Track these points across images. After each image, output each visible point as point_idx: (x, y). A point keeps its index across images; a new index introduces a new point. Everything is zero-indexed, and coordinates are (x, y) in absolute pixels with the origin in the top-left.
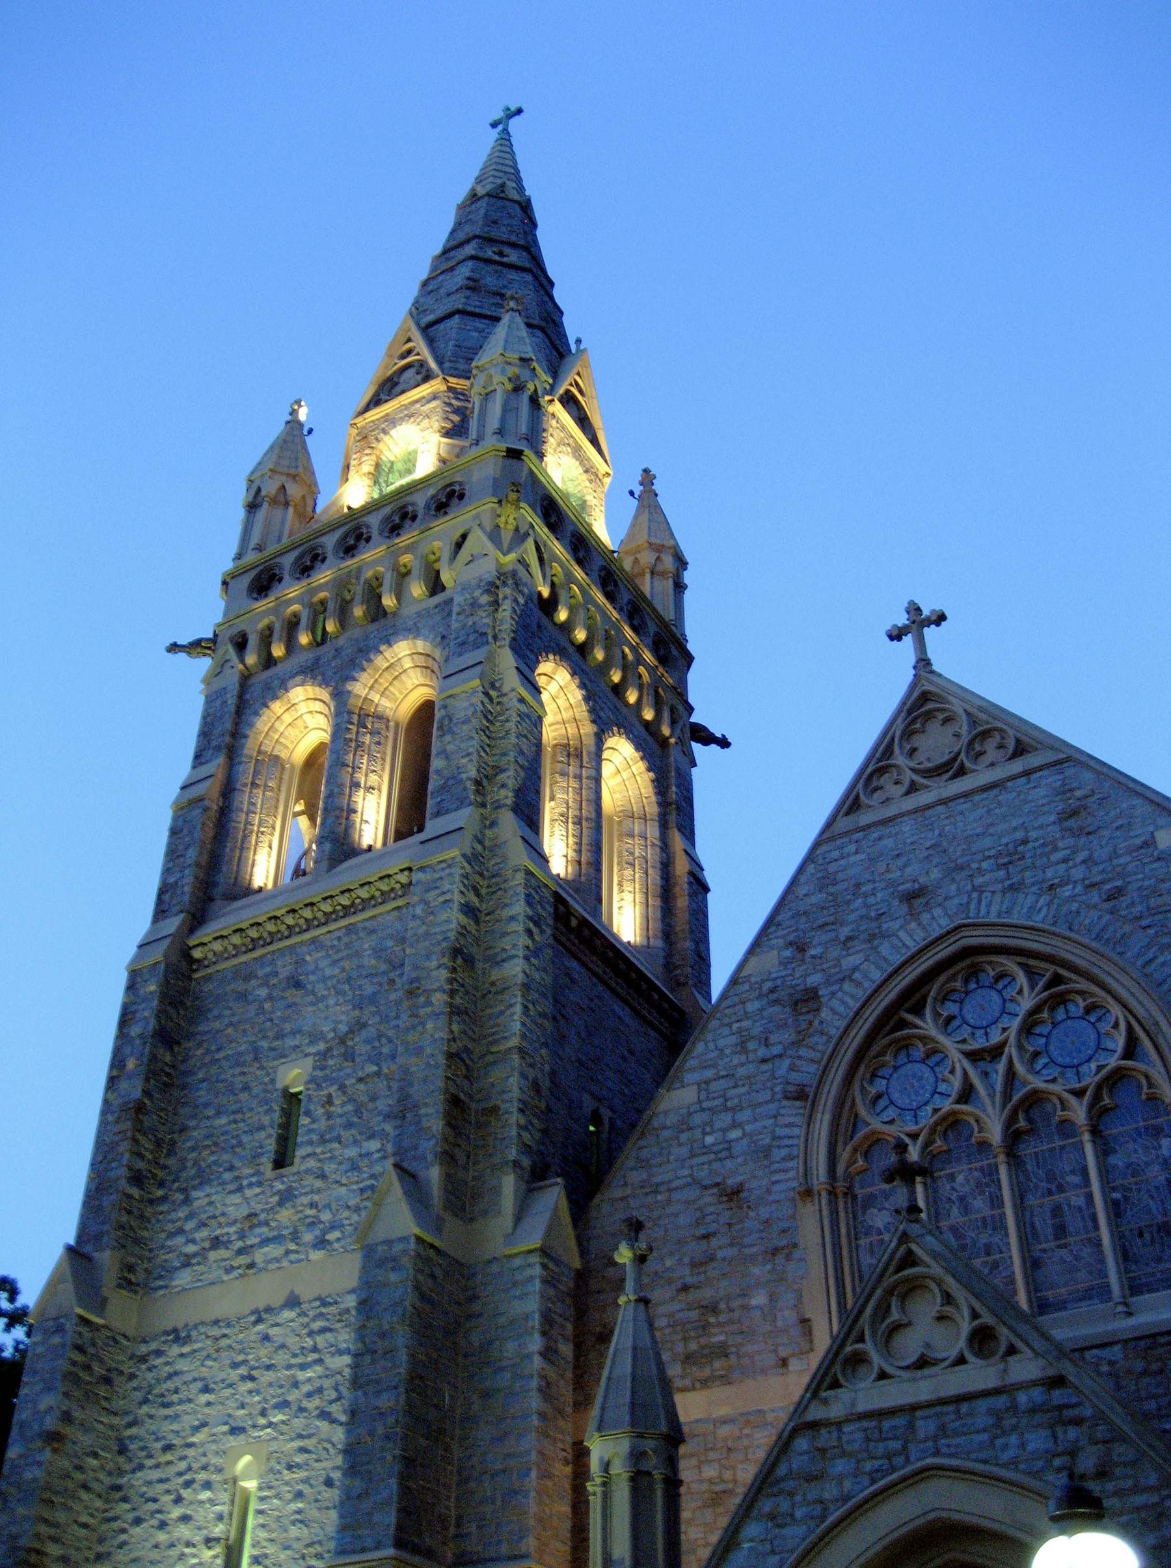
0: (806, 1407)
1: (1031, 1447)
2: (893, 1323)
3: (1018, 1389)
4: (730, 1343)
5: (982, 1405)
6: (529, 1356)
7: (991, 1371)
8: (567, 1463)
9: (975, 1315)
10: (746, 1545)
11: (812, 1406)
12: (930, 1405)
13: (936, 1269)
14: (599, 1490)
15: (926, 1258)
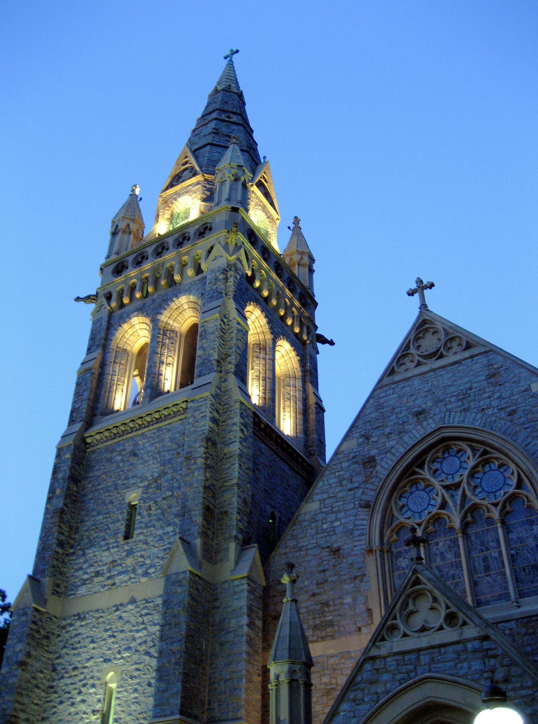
0: (369, 650)
1: (473, 668)
5: (451, 649)
6: (241, 626)
7: (455, 633)
8: (259, 675)
9: (448, 607)
10: (342, 714)
12: (427, 649)
13: (430, 586)
14: (274, 688)
15: (425, 581)
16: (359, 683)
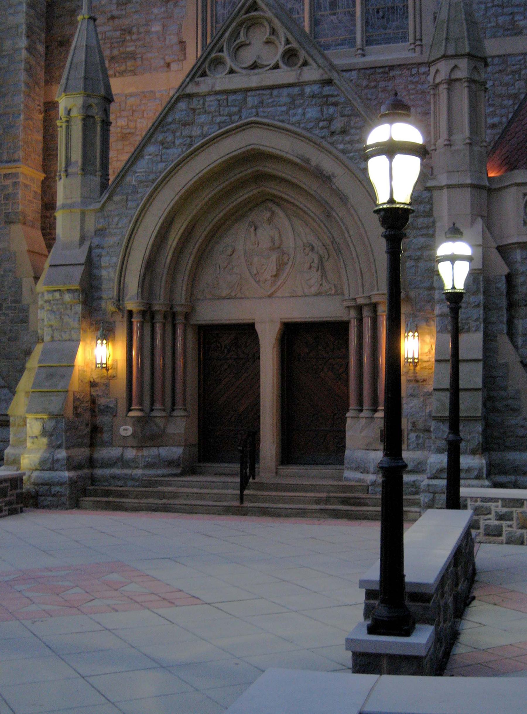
0: (186, 86)
1: (308, 115)
2: (240, 42)
3: (306, 85)
4: (137, 51)
5: (285, 91)
6: (19, 49)
7: (294, 73)
8: (41, 113)
9: (288, 42)
10: (147, 157)
11: (190, 86)
12: (256, 89)
13: (269, 14)
14: (64, 125)
15: (265, 8)
16: (171, 123)
